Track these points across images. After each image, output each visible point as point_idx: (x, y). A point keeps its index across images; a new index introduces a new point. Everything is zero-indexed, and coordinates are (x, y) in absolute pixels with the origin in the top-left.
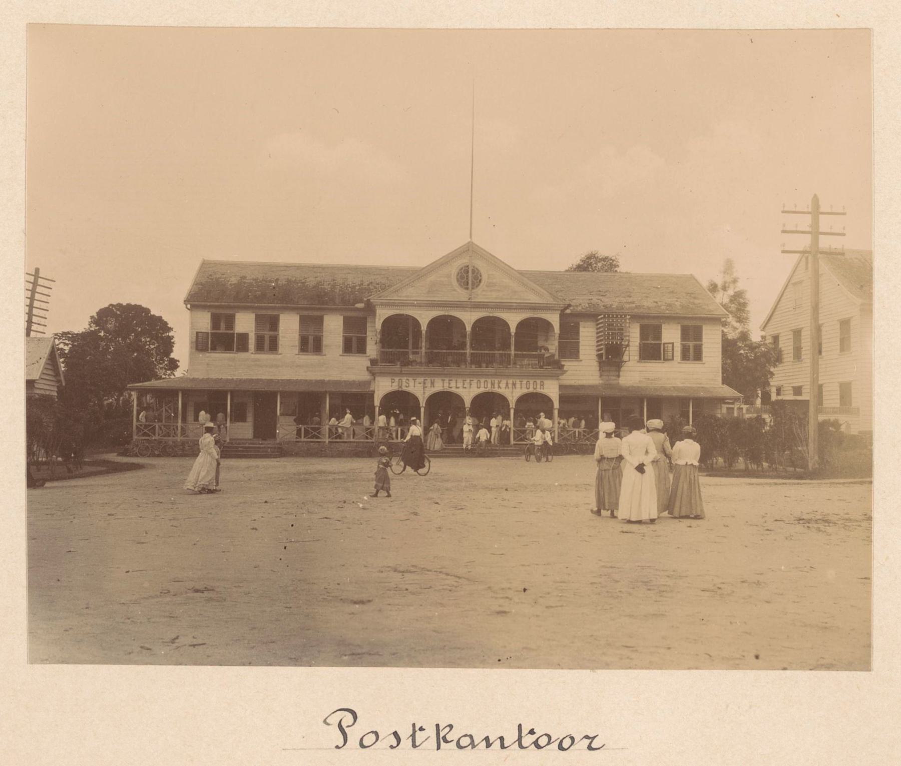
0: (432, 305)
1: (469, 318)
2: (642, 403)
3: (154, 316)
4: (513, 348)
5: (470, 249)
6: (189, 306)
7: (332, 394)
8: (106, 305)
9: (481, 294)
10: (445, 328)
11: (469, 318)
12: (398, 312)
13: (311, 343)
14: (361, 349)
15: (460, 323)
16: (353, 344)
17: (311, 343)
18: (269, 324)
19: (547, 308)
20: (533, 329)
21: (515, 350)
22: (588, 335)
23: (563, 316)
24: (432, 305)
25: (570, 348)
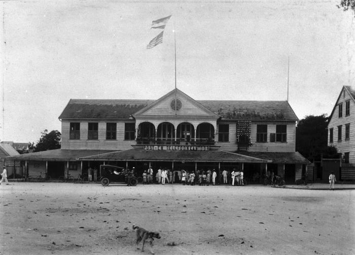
0: (159, 118)
1: (176, 123)
2: (218, 164)
3: (303, 120)
4: (162, 136)
5: (176, 92)
6: (61, 120)
7: (27, 160)
8: (319, 114)
9: (182, 112)
10: (166, 127)
11: (176, 123)
12: (164, 121)
13: (111, 134)
14: (133, 138)
15: (152, 125)
16: (129, 136)
17: (111, 134)
18: (93, 128)
19: (212, 118)
20: (205, 129)
21: (196, 137)
22: (232, 131)
23: (219, 121)
24: (159, 118)
25: (224, 137)
